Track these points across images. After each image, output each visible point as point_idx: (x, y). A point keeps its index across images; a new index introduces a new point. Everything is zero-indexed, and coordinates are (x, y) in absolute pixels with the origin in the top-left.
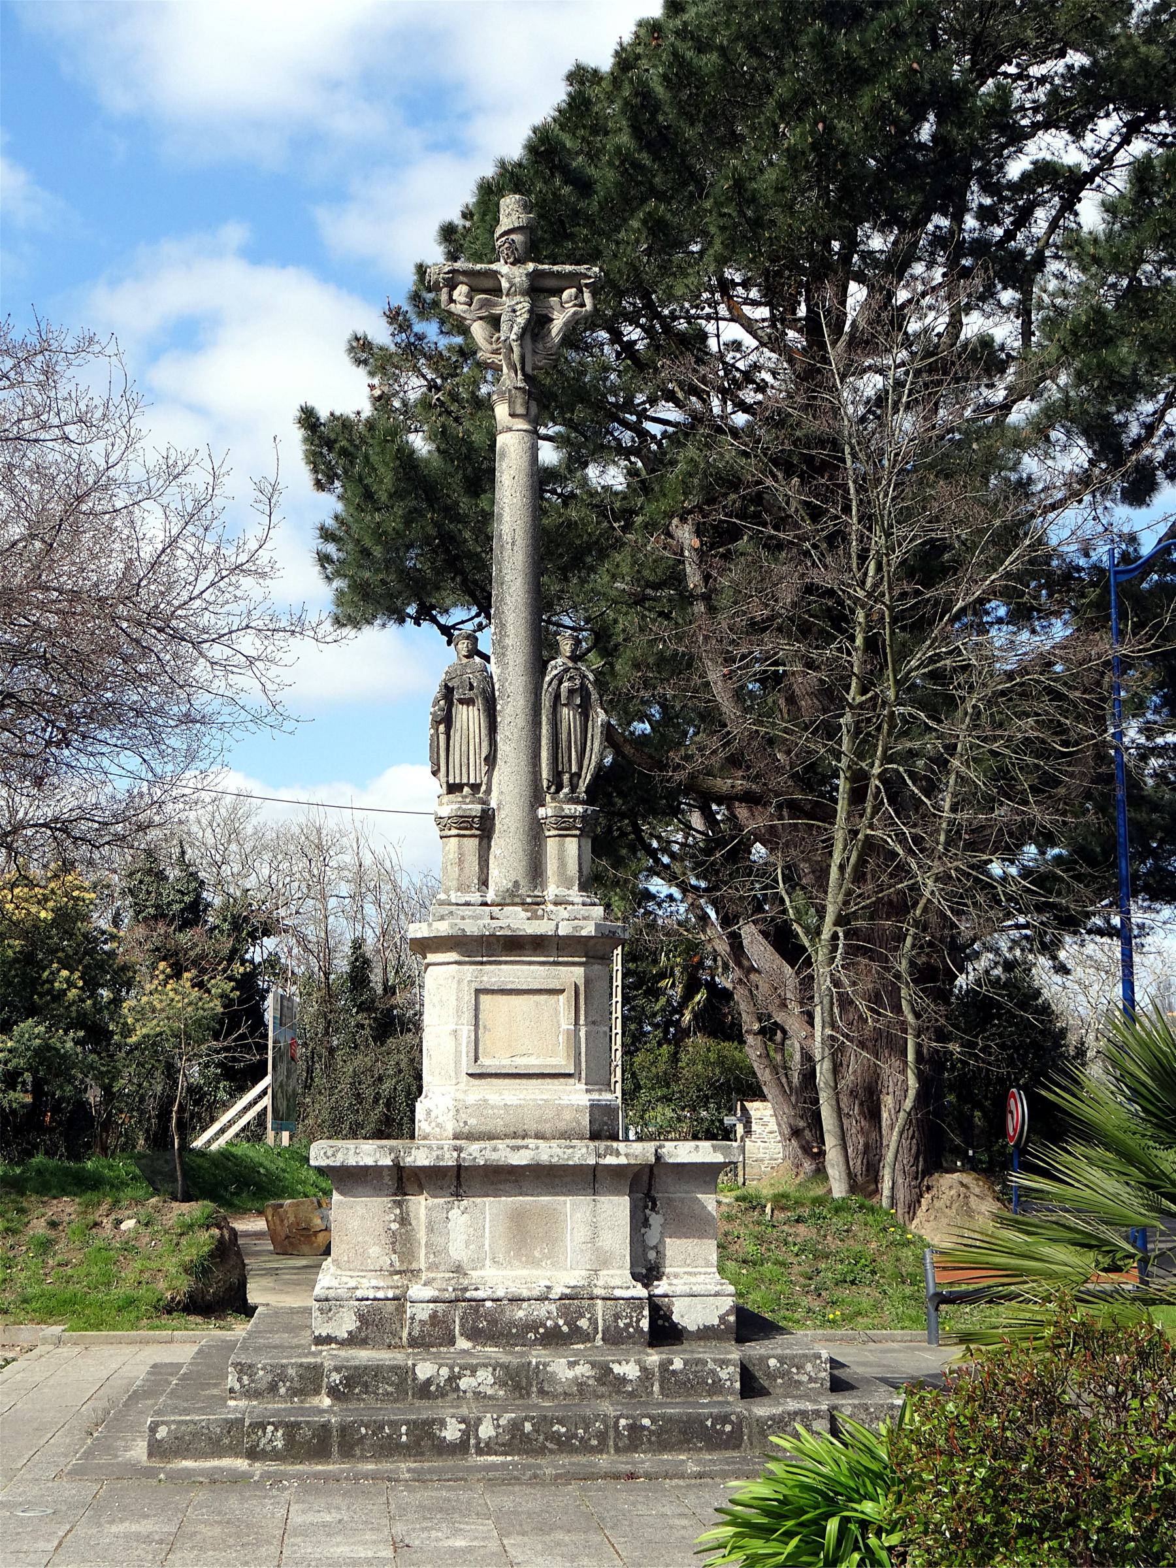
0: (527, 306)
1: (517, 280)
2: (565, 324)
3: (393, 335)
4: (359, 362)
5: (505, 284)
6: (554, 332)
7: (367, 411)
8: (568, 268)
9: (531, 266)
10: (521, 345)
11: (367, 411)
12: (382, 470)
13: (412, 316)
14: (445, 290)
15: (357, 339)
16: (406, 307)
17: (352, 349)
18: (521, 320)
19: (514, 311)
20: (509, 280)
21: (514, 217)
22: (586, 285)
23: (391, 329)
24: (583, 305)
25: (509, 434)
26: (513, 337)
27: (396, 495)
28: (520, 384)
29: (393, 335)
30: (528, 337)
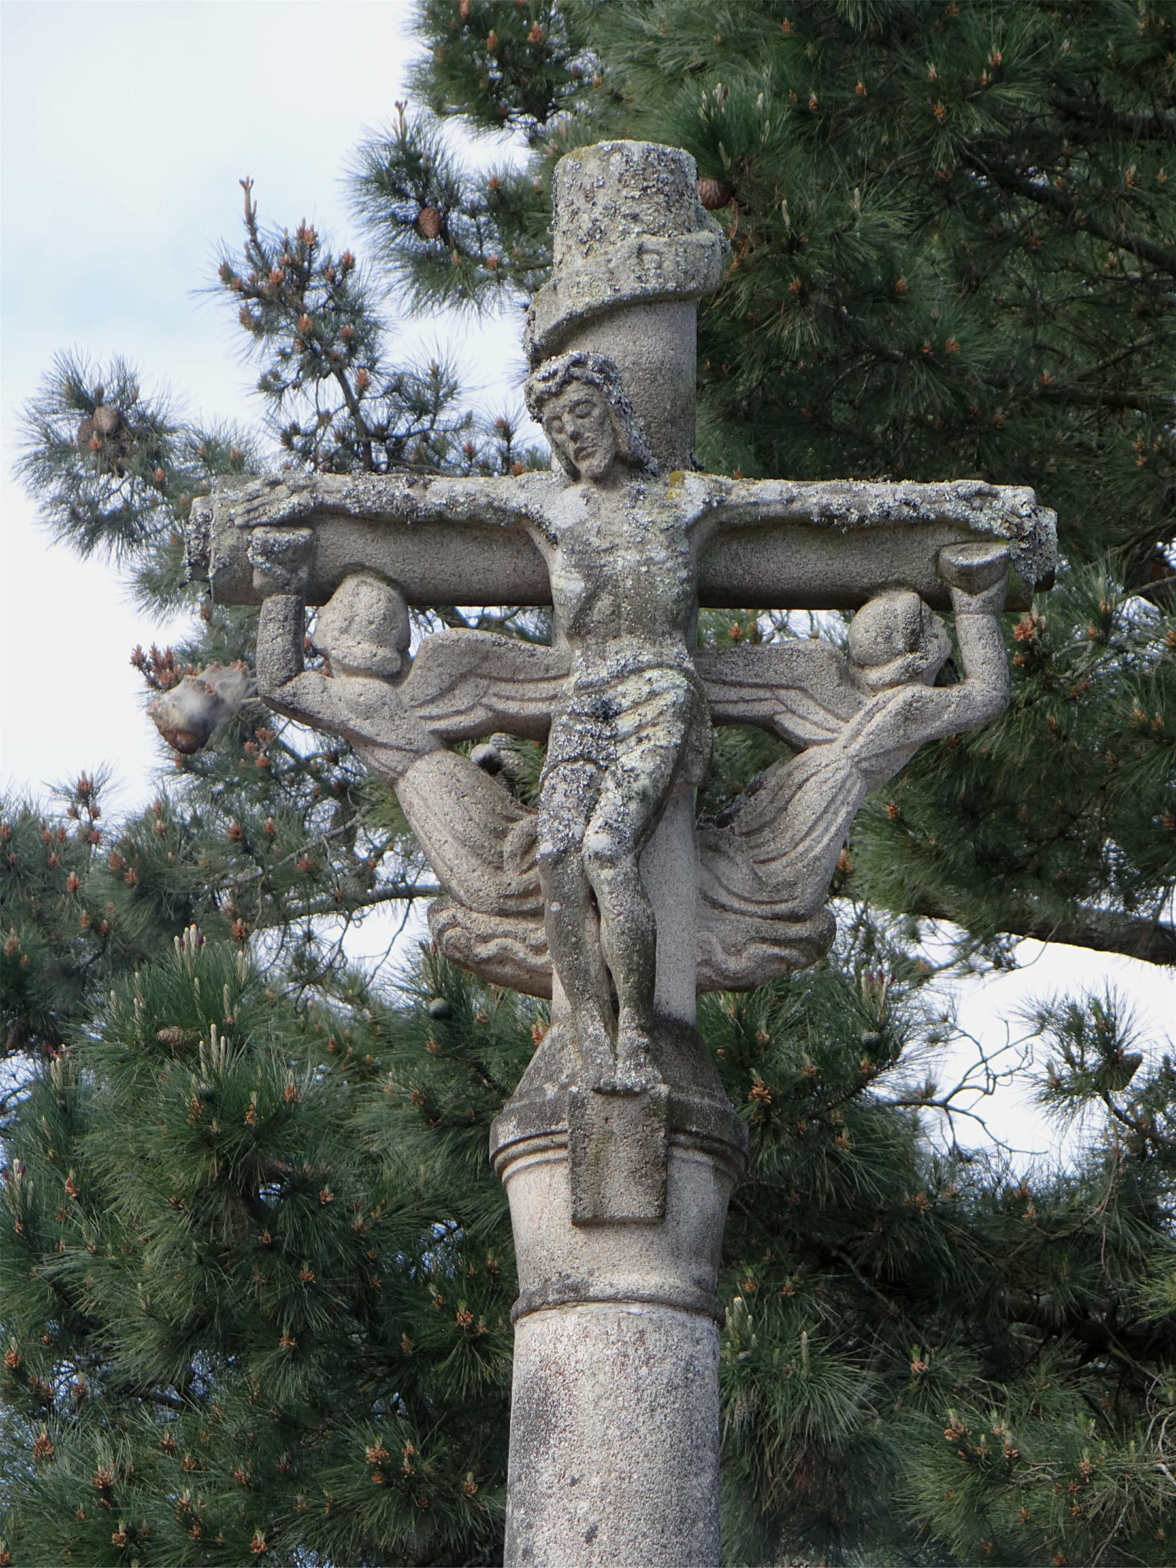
0: (670, 686)
1: (624, 560)
2: (867, 769)
3: (271, 385)
4: (91, 524)
5: (566, 582)
6: (809, 800)
7: (138, 779)
8: (881, 495)
9: (693, 492)
10: (639, 886)
11: (138, 779)
12: (130, 1197)
13: (384, 289)
14: (274, 606)
15: (79, 399)
16: (349, 232)
17: (54, 455)
18: (637, 760)
19: (606, 714)
20: (587, 563)
21: (619, 249)
22: (970, 579)
23: (263, 355)
24: (949, 672)
25: (570, 1321)
26: (596, 840)
27: (207, 1327)
28: (625, 1075)
29: (271, 385)
30: (676, 834)
